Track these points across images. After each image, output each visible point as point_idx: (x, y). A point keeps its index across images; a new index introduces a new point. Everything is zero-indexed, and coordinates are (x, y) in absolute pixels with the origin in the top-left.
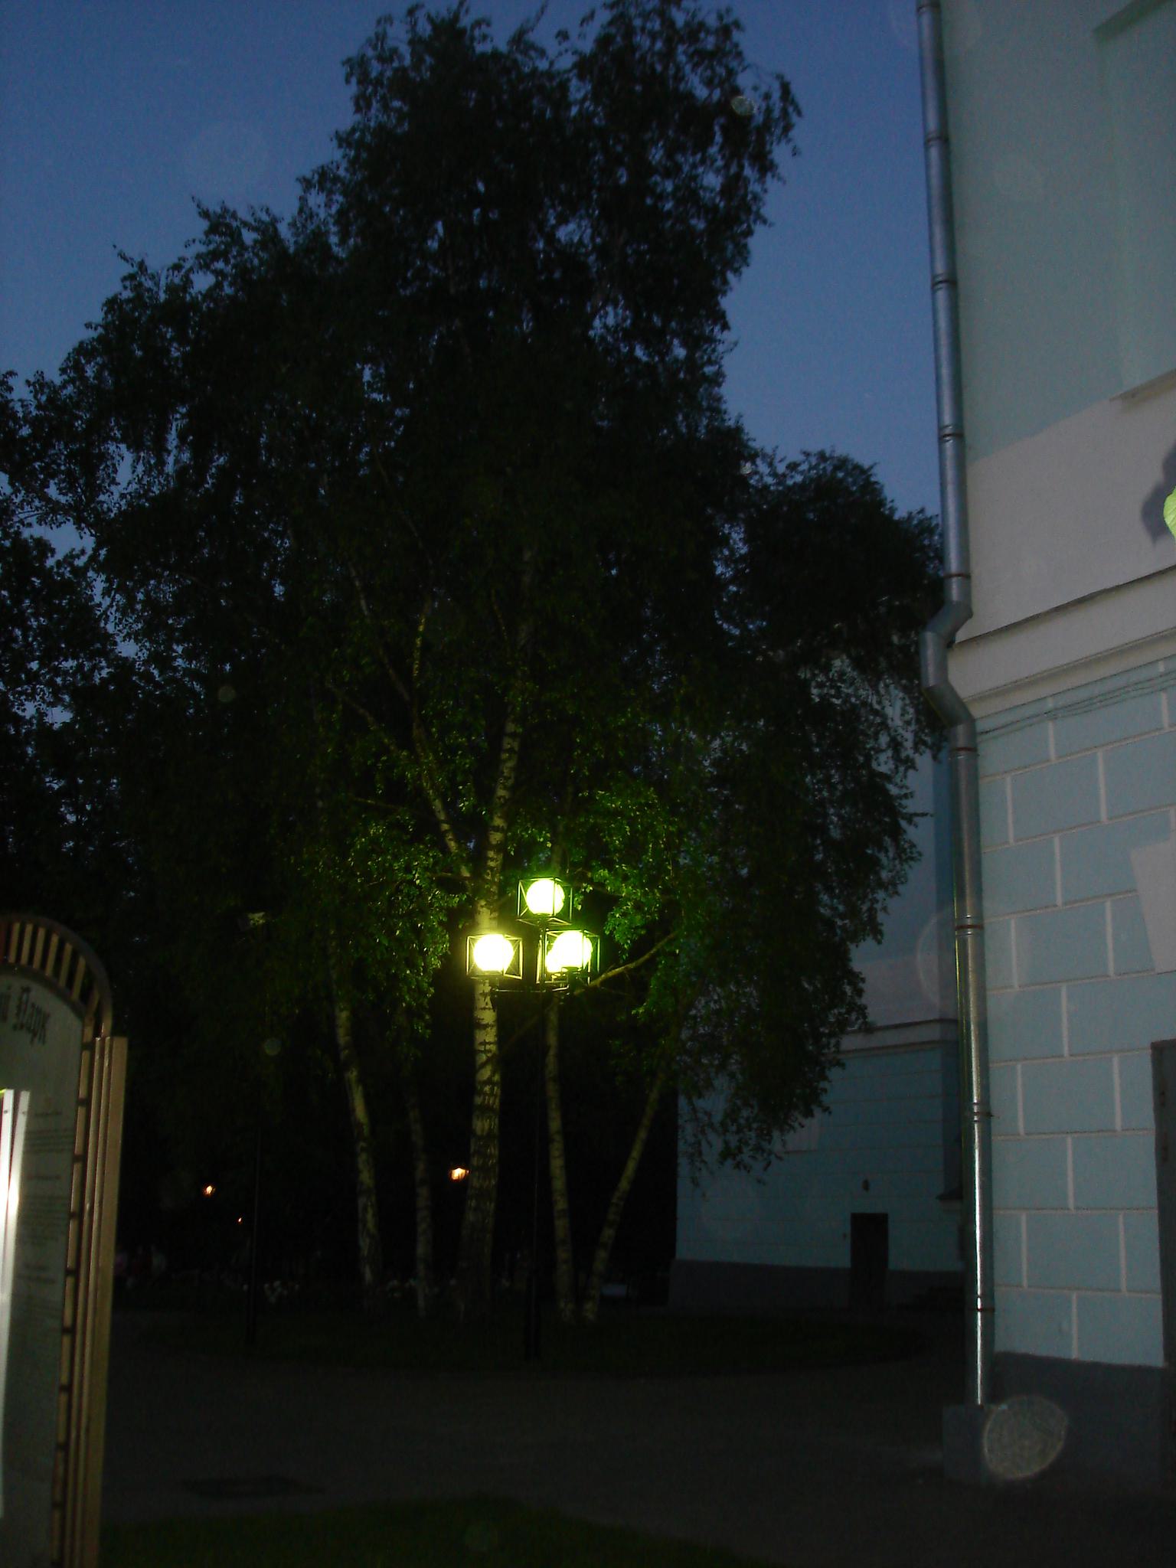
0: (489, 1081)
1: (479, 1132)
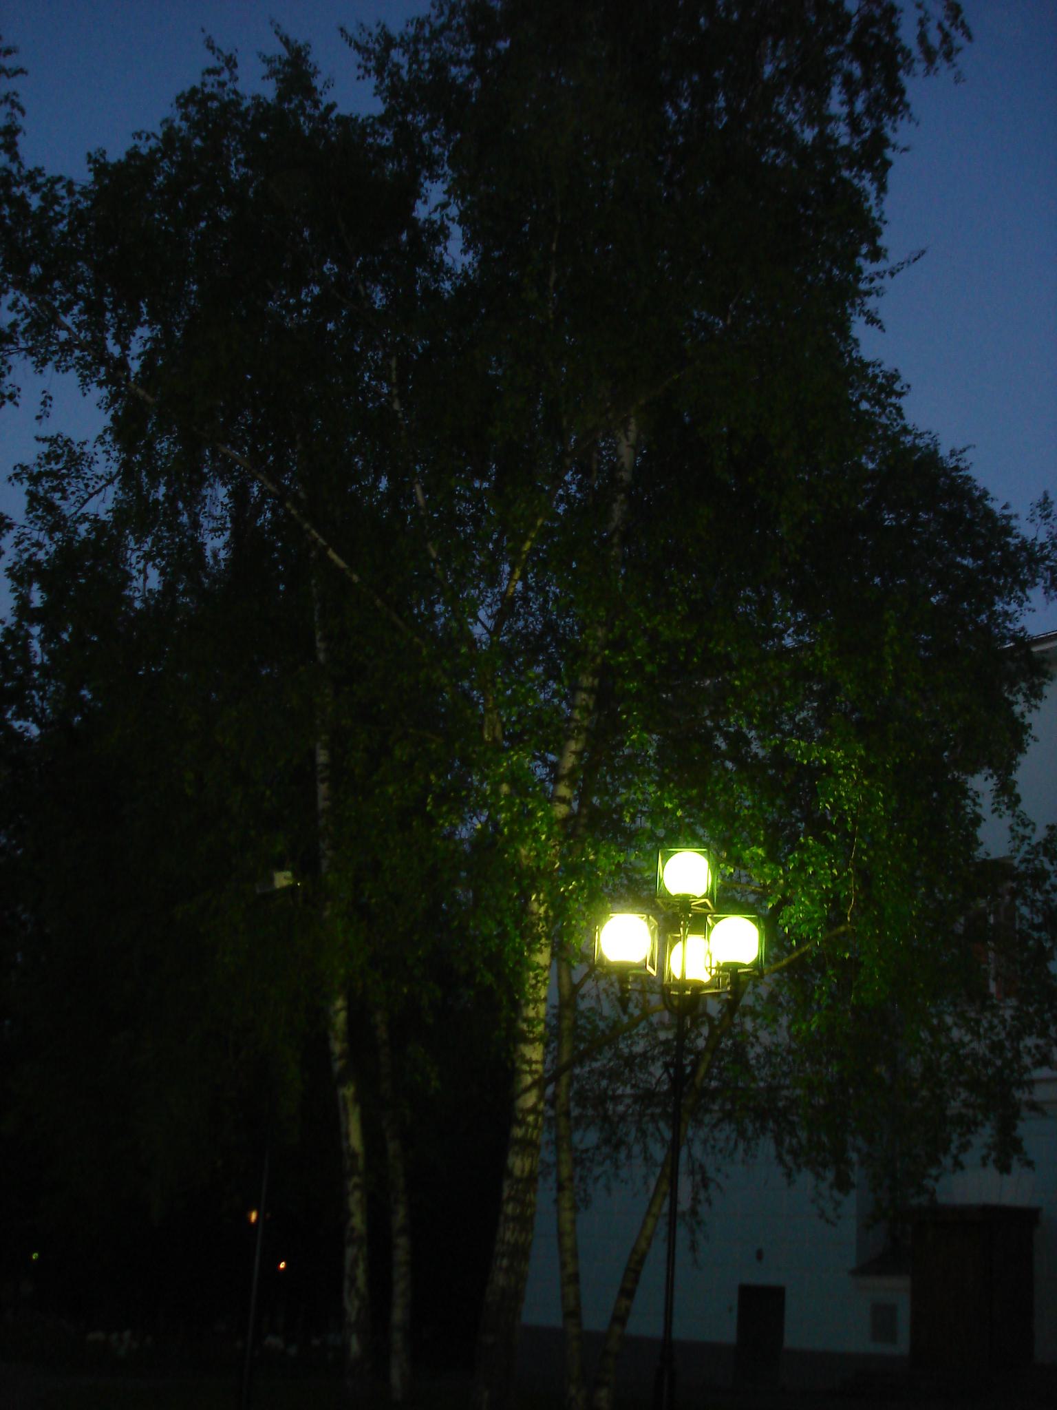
1: (517, 1172)
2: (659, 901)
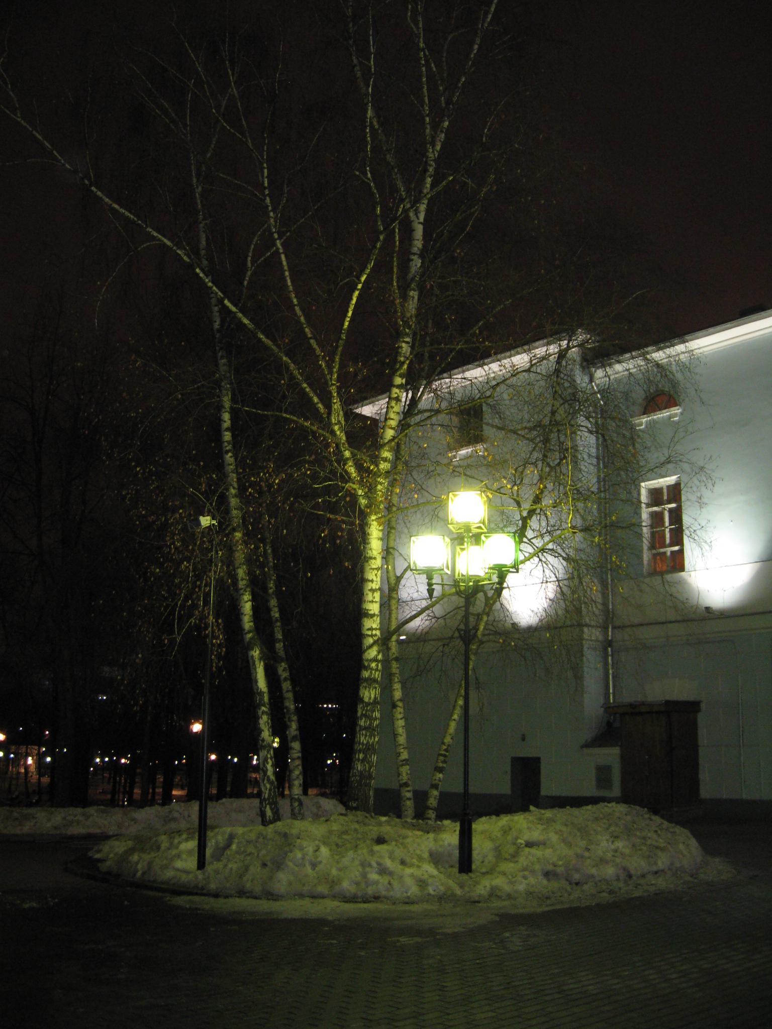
0: (375, 660)
1: (366, 700)
2: (450, 526)
